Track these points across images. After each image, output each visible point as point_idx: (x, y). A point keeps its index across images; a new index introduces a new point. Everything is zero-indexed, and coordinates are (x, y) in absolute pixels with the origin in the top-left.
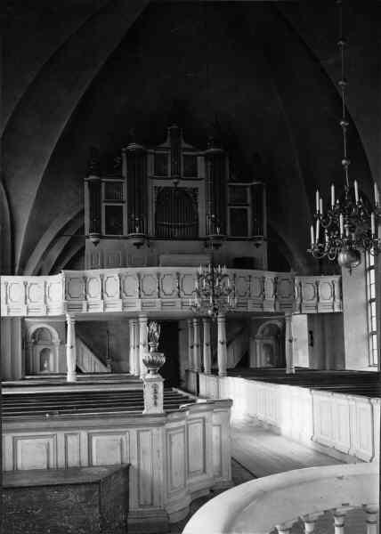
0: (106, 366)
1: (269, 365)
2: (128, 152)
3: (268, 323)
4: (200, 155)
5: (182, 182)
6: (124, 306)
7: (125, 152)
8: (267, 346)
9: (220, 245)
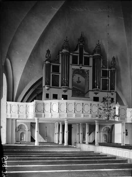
0: (45, 140)
1: (105, 142)
2: (62, 53)
3: (106, 126)
4: (91, 57)
5: (83, 67)
6: (60, 115)
7: (79, 46)
8: (105, 135)
9: (97, 93)
